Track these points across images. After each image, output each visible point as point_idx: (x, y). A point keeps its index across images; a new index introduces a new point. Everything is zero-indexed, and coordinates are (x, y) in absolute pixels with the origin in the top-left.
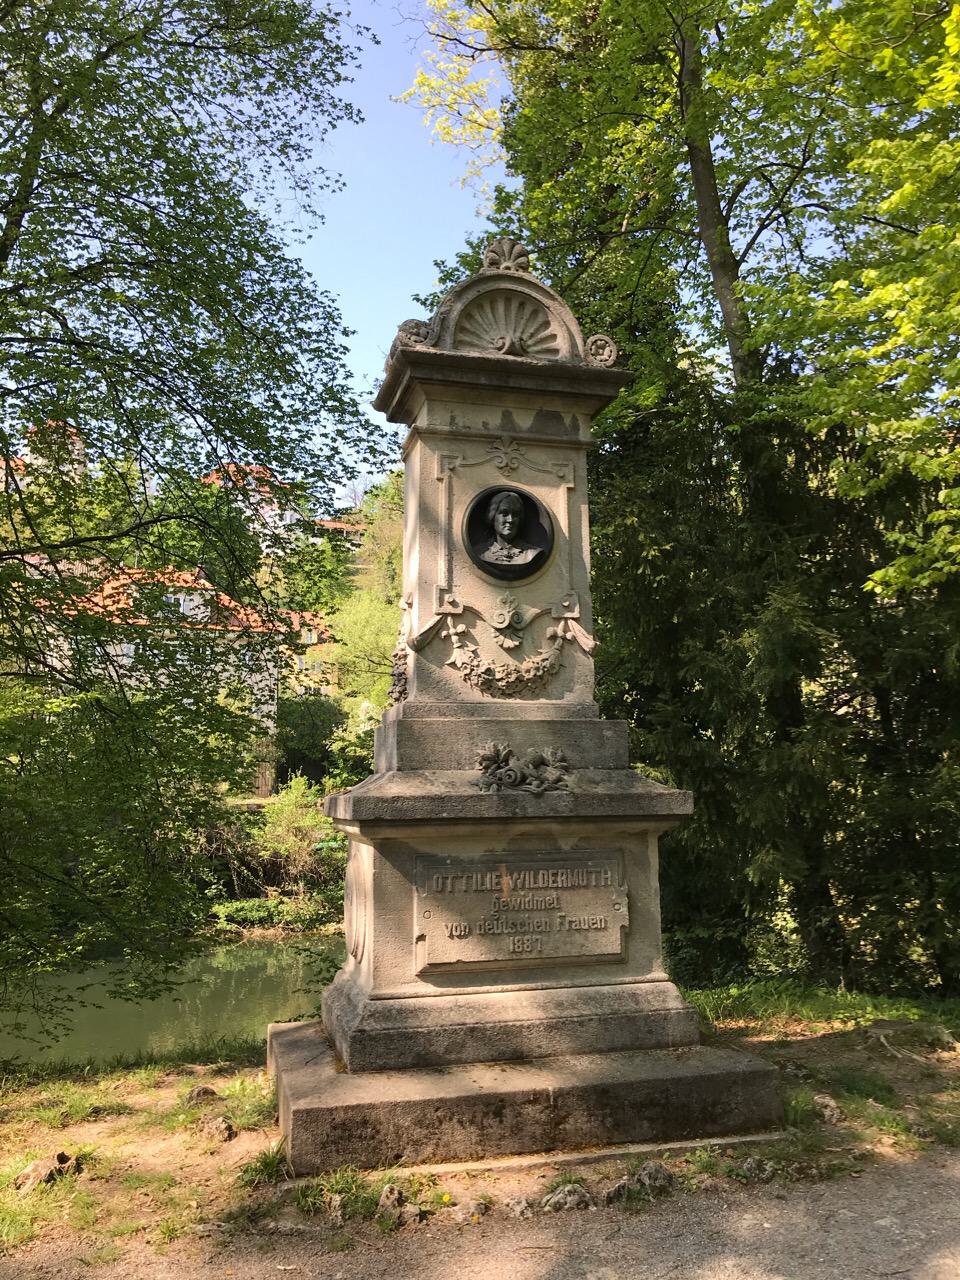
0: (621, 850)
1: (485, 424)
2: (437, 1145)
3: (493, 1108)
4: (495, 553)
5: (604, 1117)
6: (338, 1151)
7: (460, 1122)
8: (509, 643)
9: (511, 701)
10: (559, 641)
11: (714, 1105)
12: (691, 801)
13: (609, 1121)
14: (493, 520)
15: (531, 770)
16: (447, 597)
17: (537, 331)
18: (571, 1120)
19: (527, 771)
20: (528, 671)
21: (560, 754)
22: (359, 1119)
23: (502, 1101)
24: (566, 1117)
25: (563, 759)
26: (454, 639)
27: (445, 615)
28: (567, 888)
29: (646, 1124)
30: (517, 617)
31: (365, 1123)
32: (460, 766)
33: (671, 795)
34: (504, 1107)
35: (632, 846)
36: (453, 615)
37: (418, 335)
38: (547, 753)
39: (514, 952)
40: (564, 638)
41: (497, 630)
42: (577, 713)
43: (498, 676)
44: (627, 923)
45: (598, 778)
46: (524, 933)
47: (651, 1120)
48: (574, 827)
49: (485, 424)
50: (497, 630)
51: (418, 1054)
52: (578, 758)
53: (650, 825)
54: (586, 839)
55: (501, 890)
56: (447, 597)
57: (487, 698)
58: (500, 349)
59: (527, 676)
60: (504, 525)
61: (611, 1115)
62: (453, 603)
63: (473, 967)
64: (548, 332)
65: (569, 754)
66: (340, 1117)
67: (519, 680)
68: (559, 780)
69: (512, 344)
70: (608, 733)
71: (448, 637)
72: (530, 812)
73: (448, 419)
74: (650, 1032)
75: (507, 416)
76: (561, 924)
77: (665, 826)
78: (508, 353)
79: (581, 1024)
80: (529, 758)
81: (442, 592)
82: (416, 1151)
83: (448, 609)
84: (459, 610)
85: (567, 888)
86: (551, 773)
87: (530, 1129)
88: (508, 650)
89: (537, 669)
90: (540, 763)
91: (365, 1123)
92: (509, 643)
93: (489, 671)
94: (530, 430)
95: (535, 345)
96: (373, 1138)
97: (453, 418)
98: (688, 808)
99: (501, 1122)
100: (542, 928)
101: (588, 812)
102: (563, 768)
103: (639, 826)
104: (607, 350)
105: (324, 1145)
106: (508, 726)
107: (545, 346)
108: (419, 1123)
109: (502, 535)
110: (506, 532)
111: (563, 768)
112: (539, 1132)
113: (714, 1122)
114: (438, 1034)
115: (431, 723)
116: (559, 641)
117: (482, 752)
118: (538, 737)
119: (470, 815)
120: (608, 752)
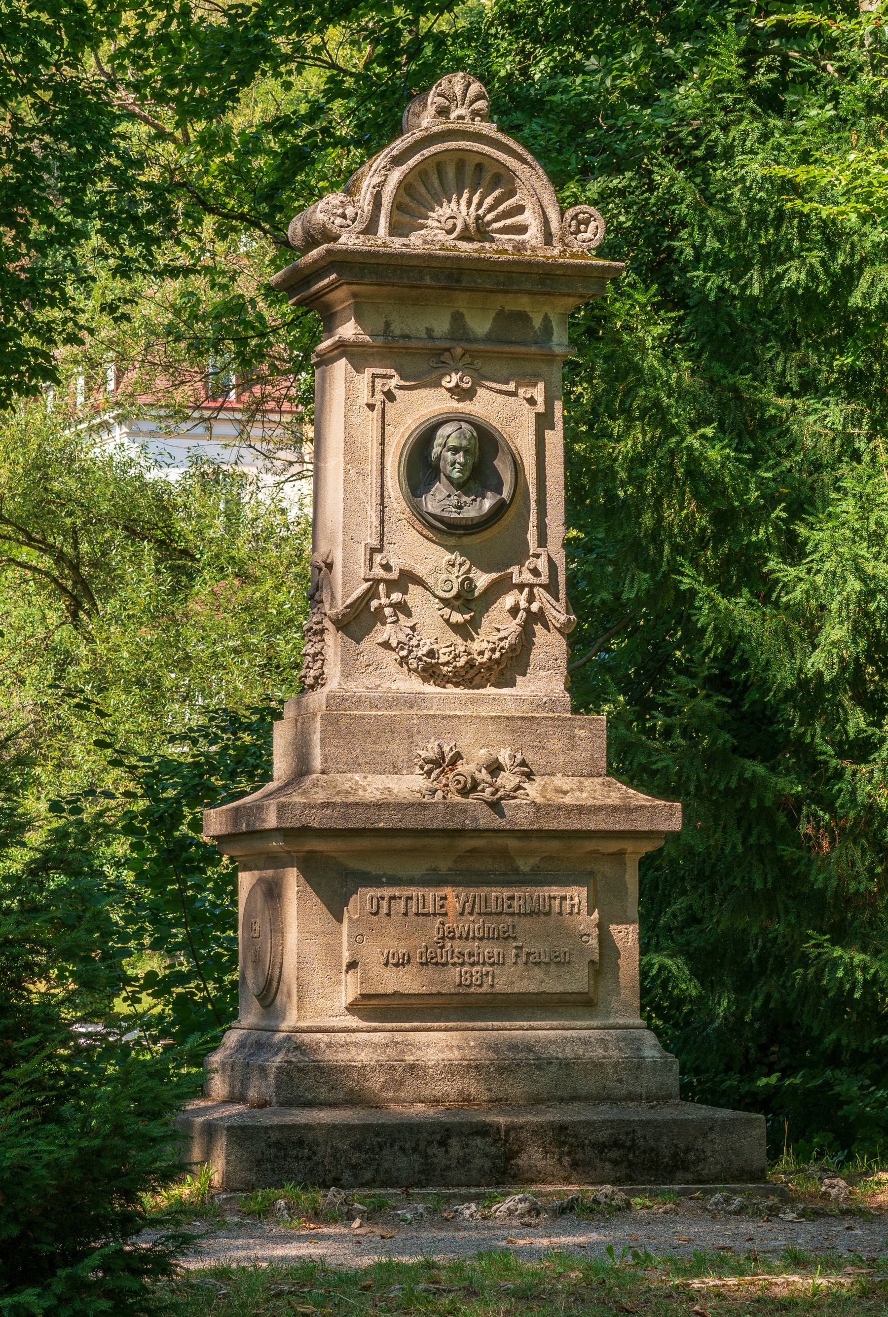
0: (592, 874)
1: (429, 331)
2: (377, 1170)
3: (438, 1137)
4: (439, 500)
5: (562, 1154)
6: (273, 1170)
7: (402, 1149)
8: (457, 618)
9: (481, 691)
10: (522, 614)
11: (688, 1150)
12: (679, 815)
13: (566, 1160)
14: (439, 458)
15: (484, 775)
16: (378, 558)
17: (498, 202)
18: (524, 1156)
19: (479, 776)
20: (481, 653)
21: (519, 756)
22: (295, 1139)
23: (447, 1130)
24: (518, 1152)
25: (523, 763)
26: (388, 611)
27: (377, 582)
28: (525, 914)
29: (608, 1166)
30: (468, 584)
31: (301, 1143)
32: (396, 770)
33: (654, 807)
34: (449, 1137)
35: (606, 869)
36: (387, 582)
37: (344, 216)
38: (504, 756)
39: (460, 985)
40: (528, 610)
41: (442, 600)
42: (542, 706)
43: (443, 659)
44: (596, 958)
45: (566, 787)
46: (473, 964)
47: (615, 1163)
48: (535, 844)
49: (429, 331)
50: (442, 600)
51: (352, 1090)
52: (543, 762)
53: (629, 846)
54: (551, 858)
55: (445, 914)
56: (378, 558)
57: (430, 689)
58: (450, 232)
59: (479, 660)
60: (454, 464)
61: (569, 1154)
62: (387, 567)
63: (412, 1001)
64: (511, 202)
65: (530, 758)
66: (274, 1136)
67: (470, 664)
68: (519, 788)
69: (466, 227)
70: (582, 733)
71: (381, 608)
72: (483, 824)
73: (381, 326)
74: (620, 1081)
75: (457, 318)
76: (517, 956)
77: (647, 847)
78: (461, 238)
79: (539, 1067)
80: (482, 761)
81: (373, 551)
82: (355, 1176)
83: (379, 572)
84: (394, 575)
85: (525, 914)
86: (507, 780)
87: (478, 1162)
88: (456, 628)
89: (493, 651)
90: (495, 768)
91: (301, 1143)
92: (457, 618)
93: (431, 653)
94: (488, 339)
95: (497, 219)
96: (309, 1159)
97: (387, 325)
98: (676, 824)
99: (447, 1152)
100: (495, 959)
101: (552, 825)
102: (523, 774)
103: (612, 846)
104: (592, 225)
105: (259, 1162)
106: (455, 722)
107: (509, 222)
108: (357, 1147)
109: (449, 478)
110: (456, 475)
111: (523, 774)
112: (488, 1165)
113: (686, 1169)
114: (374, 1069)
115: (361, 718)
116: (522, 614)
117: (424, 754)
118: (493, 736)
119: (412, 825)
120: (580, 756)
